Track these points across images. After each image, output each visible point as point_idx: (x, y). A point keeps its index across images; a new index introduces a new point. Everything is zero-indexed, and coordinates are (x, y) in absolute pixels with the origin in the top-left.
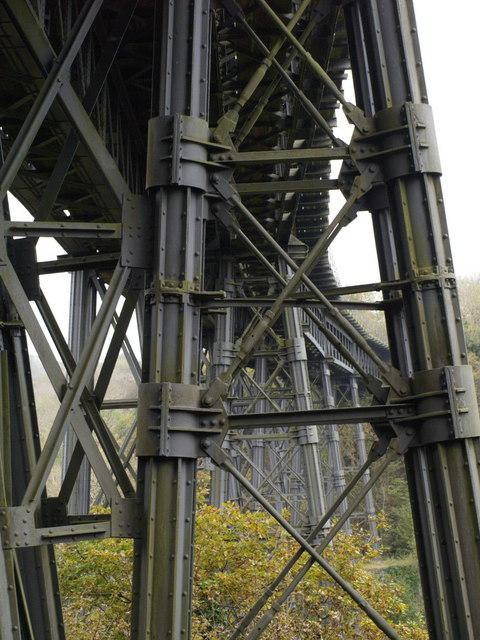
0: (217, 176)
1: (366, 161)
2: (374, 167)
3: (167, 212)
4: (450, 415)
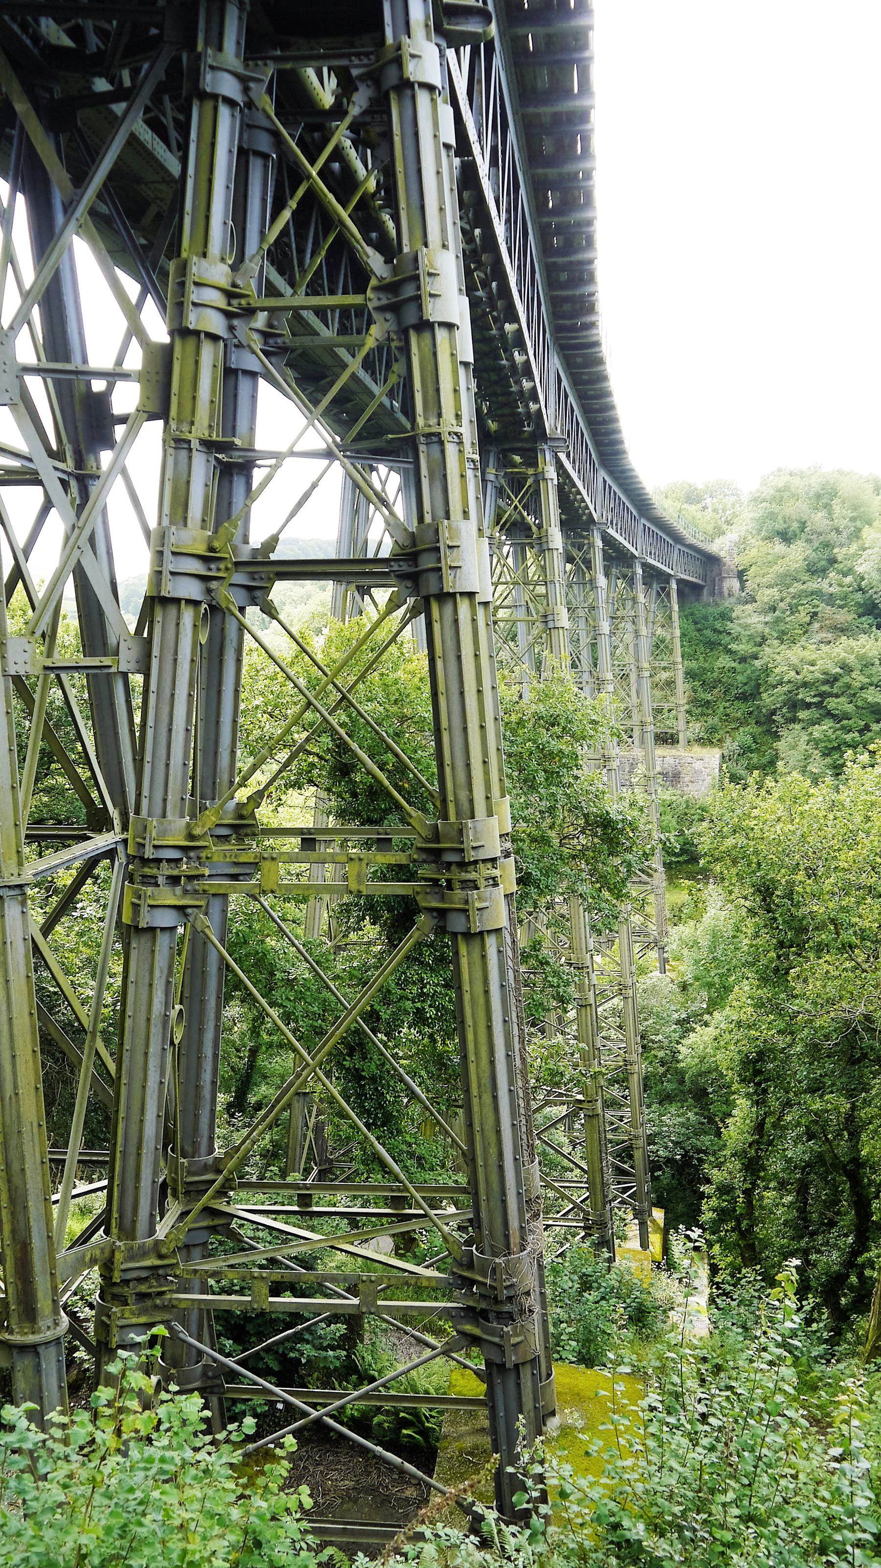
0: (236, 322)
1: (381, 309)
2: (388, 316)
3: (182, 356)
4: (440, 569)
